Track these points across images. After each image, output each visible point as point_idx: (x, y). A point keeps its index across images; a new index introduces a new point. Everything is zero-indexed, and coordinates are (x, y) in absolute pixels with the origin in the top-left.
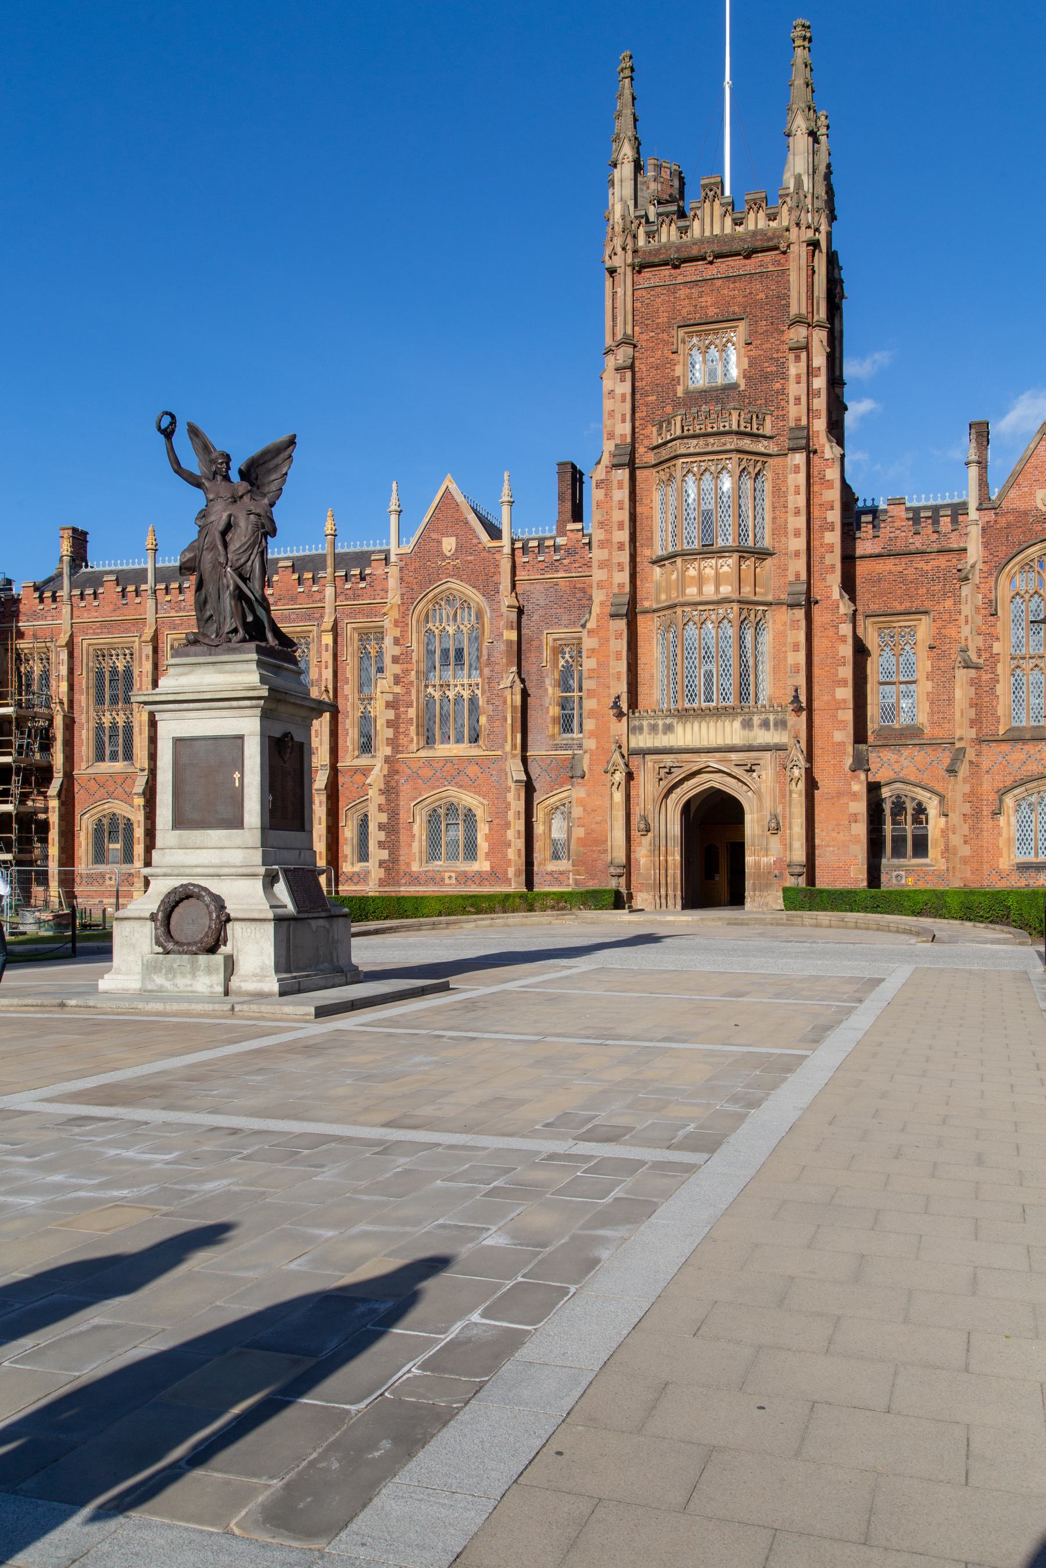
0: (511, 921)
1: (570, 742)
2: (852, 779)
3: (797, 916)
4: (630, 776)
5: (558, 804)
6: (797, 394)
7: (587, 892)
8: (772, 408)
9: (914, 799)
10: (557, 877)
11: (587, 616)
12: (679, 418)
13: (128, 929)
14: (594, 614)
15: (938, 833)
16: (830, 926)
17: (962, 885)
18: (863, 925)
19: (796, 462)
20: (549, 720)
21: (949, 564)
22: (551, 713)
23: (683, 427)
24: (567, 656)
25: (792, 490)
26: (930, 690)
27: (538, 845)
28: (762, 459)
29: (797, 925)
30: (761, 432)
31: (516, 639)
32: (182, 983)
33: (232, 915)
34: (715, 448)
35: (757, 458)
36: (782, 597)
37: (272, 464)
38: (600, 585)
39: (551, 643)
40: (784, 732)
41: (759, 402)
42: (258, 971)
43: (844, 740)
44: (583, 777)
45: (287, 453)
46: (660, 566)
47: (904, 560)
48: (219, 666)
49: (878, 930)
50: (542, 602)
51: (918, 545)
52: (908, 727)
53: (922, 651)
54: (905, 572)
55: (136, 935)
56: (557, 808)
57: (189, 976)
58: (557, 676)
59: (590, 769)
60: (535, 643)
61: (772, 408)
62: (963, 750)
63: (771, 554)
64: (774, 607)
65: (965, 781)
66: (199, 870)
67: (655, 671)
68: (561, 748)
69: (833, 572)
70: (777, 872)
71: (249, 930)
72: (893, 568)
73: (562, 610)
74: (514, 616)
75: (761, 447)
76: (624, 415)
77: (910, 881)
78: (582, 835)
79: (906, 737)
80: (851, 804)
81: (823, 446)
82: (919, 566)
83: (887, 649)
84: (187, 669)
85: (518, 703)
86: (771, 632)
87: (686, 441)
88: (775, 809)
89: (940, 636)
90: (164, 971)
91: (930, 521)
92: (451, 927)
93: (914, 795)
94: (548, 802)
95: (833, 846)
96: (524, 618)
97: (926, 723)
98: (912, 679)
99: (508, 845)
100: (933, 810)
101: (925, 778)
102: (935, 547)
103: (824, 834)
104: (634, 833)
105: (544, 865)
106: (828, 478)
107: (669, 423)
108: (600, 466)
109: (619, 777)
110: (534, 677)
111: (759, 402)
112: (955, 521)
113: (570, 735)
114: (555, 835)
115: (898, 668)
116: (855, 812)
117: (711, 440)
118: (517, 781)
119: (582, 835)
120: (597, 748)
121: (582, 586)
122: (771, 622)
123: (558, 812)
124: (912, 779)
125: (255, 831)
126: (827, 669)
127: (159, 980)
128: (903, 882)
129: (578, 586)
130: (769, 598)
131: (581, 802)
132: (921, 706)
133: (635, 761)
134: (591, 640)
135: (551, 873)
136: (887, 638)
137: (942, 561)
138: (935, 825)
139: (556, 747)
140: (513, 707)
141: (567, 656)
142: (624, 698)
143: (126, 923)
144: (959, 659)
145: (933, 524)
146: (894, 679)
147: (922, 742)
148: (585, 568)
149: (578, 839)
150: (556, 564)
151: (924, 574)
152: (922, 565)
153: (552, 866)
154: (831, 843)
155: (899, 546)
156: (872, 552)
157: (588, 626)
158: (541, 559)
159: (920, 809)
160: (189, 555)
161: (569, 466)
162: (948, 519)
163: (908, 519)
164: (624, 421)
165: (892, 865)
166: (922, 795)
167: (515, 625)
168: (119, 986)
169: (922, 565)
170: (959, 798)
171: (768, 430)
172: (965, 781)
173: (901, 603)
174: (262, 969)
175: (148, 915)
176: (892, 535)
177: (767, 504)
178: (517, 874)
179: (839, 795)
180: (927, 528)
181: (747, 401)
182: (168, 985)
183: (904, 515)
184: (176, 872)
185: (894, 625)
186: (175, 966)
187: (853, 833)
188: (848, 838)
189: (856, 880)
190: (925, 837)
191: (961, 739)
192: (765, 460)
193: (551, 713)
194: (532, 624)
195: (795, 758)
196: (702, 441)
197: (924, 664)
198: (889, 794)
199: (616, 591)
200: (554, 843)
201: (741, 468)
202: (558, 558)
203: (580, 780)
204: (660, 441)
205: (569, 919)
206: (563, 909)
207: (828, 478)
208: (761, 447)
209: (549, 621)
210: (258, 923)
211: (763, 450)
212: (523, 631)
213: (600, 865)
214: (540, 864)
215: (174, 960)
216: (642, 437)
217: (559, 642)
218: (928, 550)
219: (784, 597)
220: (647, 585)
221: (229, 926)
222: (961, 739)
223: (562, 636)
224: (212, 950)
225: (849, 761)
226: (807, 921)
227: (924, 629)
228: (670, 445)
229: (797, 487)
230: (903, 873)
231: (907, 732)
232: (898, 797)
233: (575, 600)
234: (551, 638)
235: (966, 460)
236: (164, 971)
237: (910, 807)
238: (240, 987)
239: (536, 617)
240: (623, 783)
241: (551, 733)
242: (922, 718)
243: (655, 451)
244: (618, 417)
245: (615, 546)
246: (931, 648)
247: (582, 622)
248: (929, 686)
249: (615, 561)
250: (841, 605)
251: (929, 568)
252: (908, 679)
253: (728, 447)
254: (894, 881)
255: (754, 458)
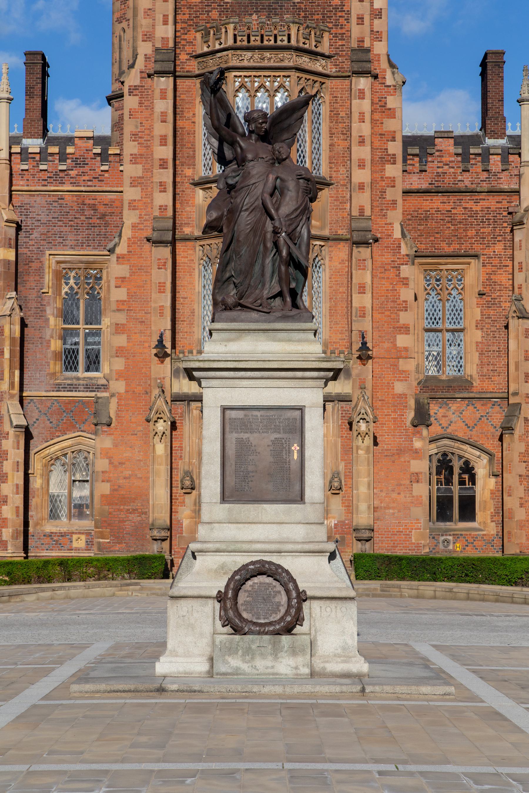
0: (73, 592)
1: (75, 382)
2: (414, 434)
3: (393, 586)
4: (174, 426)
5: (59, 453)
6: (361, 13)
7: (136, 558)
8: (330, 25)
9: (460, 457)
10: (62, 539)
11: (117, 240)
12: (232, 26)
13: (185, 609)
14: (124, 238)
15: (487, 495)
16: (435, 598)
17: (518, 551)
18: (477, 596)
19: (361, 87)
20: (50, 355)
21: (499, 205)
22: (53, 348)
23: (235, 35)
24: (72, 282)
25: (355, 116)
26: (480, 340)
27: (33, 502)
28: (320, 79)
29: (395, 596)
30: (319, 50)
31: (13, 259)
32: (262, 664)
33: (309, 593)
34: (272, 64)
35: (316, 79)
36: (340, 232)
37: (288, 122)
38: (132, 205)
39: (54, 266)
40: (346, 382)
41: (315, 17)
42: (339, 651)
43: (406, 392)
44: (109, 425)
45: (299, 114)
46: (203, 189)
47: (453, 198)
48: (271, 334)
49: (497, 601)
50: (43, 218)
51: (467, 183)
52: (455, 379)
53: (472, 299)
54: (454, 211)
55: (195, 615)
56: (57, 458)
57: (270, 658)
58: (59, 304)
59: (118, 416)
60: (34, 265)
61: (330, 25)
62: (518, 405)
63: (328, 185)
64: (330, 243)
65: (521, 439)
66: (259, 546)
67: (196, 306)
68: (65, 389)
69: (395, 209)
70: (338, 536)
71: (328, 609)
72: (441, 206)
73: (68, 229)
74: (12, 232)
75: (318, 66)
76: (166, 17)
77: (458, 547)
78: (108, 492)
79: (454, 390)
80: (413, 462)
81: (385, 71)
82: (468, 206)
83: (433, 294)
84: (233, 335)
85: (18, 334)
86: (327, 270)
87: (239, 52)
88: (337, 467)
89: (489, 282)
90: (240, 652)
91: (479, 159)
92: (13, 600)
93: (462, 453)
94: (47, 451)
95: (393, 508)
96: (22, 234)
97: (474, 373)
98: (459, 327)
99: (4, 501)
100: (481, 469)
101: (474, 435)
102: (485, 186)
103: (384, 494)
104: (178, 491)
105: (43, 526)
106: (389, 106)
107: (218, 30)
108: (133, 71)
109: (162, 426)
110: (33, 305)
111: (315, 17)
112: (505, 161)
113: (74, 374)
114: (53, 490)
115: (444, 314)
116: (417, 471)
117: (267, 54)
118: (17, 427)
119: (108, 492)
120: (127, 391)
121: (92, 202)
122: (327, 259)
123: (58, 463)
124: (460, 435)
125: (318, 506)
126: (387, 313)
127: (235, 662)
128: (451, 547)
129: (87, 202)
130: (326, 233)
131: (106, 454)
132: (469, 356)
133: (180, 407)
134: (121, 267)
135: (50, 535)
136: (433, 281)
137: (492, 202)
138: (485, 486)
139: (58, 387)
140: (12, 339)
141: (72, 282)
142: (168, 336)
143: (183, 602)
144: (514, 308)
145: (483, 161)
146: (440, 326)
147: (472, 395)
148: (96, 181)
149: (102, 496)
150: (62, 174)
151: (473, 214)
152: (470, 205)
153: (49, 527)
154: (391, 505)
155: (447, 182)
156: (419, 187)
157: (118, 250)
158: (42, 167)
159: (468, 469)
160: (214, 215)
161: (39, 57)
162: (498, 158)
163: (457, 155)
164: (165, 23)
165: (439, 529)
166: (471, 453)
167: (13, 242)
168: (181, 669)
169: (470, 205)
170: (516, 458)
171: (325, 48)
172: (521, 439)
173: (449, 244)
174: (344, 649)
175: (215, 593)
176: (440, 170)
177: (324, 128)
178: (15, 537)
179: (400, 452)
180: (477, 166)
181: (303, 14)
182: (245, 667)
183: (452, 149)
184: (232, 547)
185: (441, 267)
186: (254, 647)
187: (415, 493)
188: (409, 500)
189: (418, 546)
190: (472, 499)
191: (516, 394)
192: (323, 80)
193: (53, 348)
194: (31, 243)
195: (363, 411)
196: (257, 55)
197: (473, 312)
198: (435, 451)
199: (157, 213)
200: (53, 500)
201: (300, 87)
202: (64, 168)
203: (105, 428)
204: (206, 49)
205: (135, 590)
206: (105, 578)
207: (389, 106)
208: (318, 66)
209: (51, 240)
210: (340, 602)
211: (320, 69)
212: (20, 251)
213: (128, 526)
214: (37, 524)
215: (252, 641)
216: (183, 42)
217: (63, 265)
218: (479, 189)
219: (343, 232)
220: (188, 209)
221: (306, 606)
222: (516, 394)
223: (68, 258)
224: (289, 630)
225: (411, 415)
226: (406, 592)
227: (473, 273)
228: (219, 55)
229: (362, 114)
230: (451, 538)
231: (455, 384)
232: (445, 455)
233: (83, 218)
234: (53, 259)
235: (519, 97)
236: (240, 652)
237: (457, 465)
238: (324, 668)
239: (35, 235)
240: (168, 433)
241: (52, 371)
242: (471, 369)
243: (200, 60)
244: (160, 18)
245: (157, 163)
246: (481, 294)
247: (110, 245)
248: (478, 335)
249: (156, 179)
250: (403, 245)
251: (479, 208)
252: (454, 327)
253: (286, 64)
254: (441, 546)
255: (312, 78)
